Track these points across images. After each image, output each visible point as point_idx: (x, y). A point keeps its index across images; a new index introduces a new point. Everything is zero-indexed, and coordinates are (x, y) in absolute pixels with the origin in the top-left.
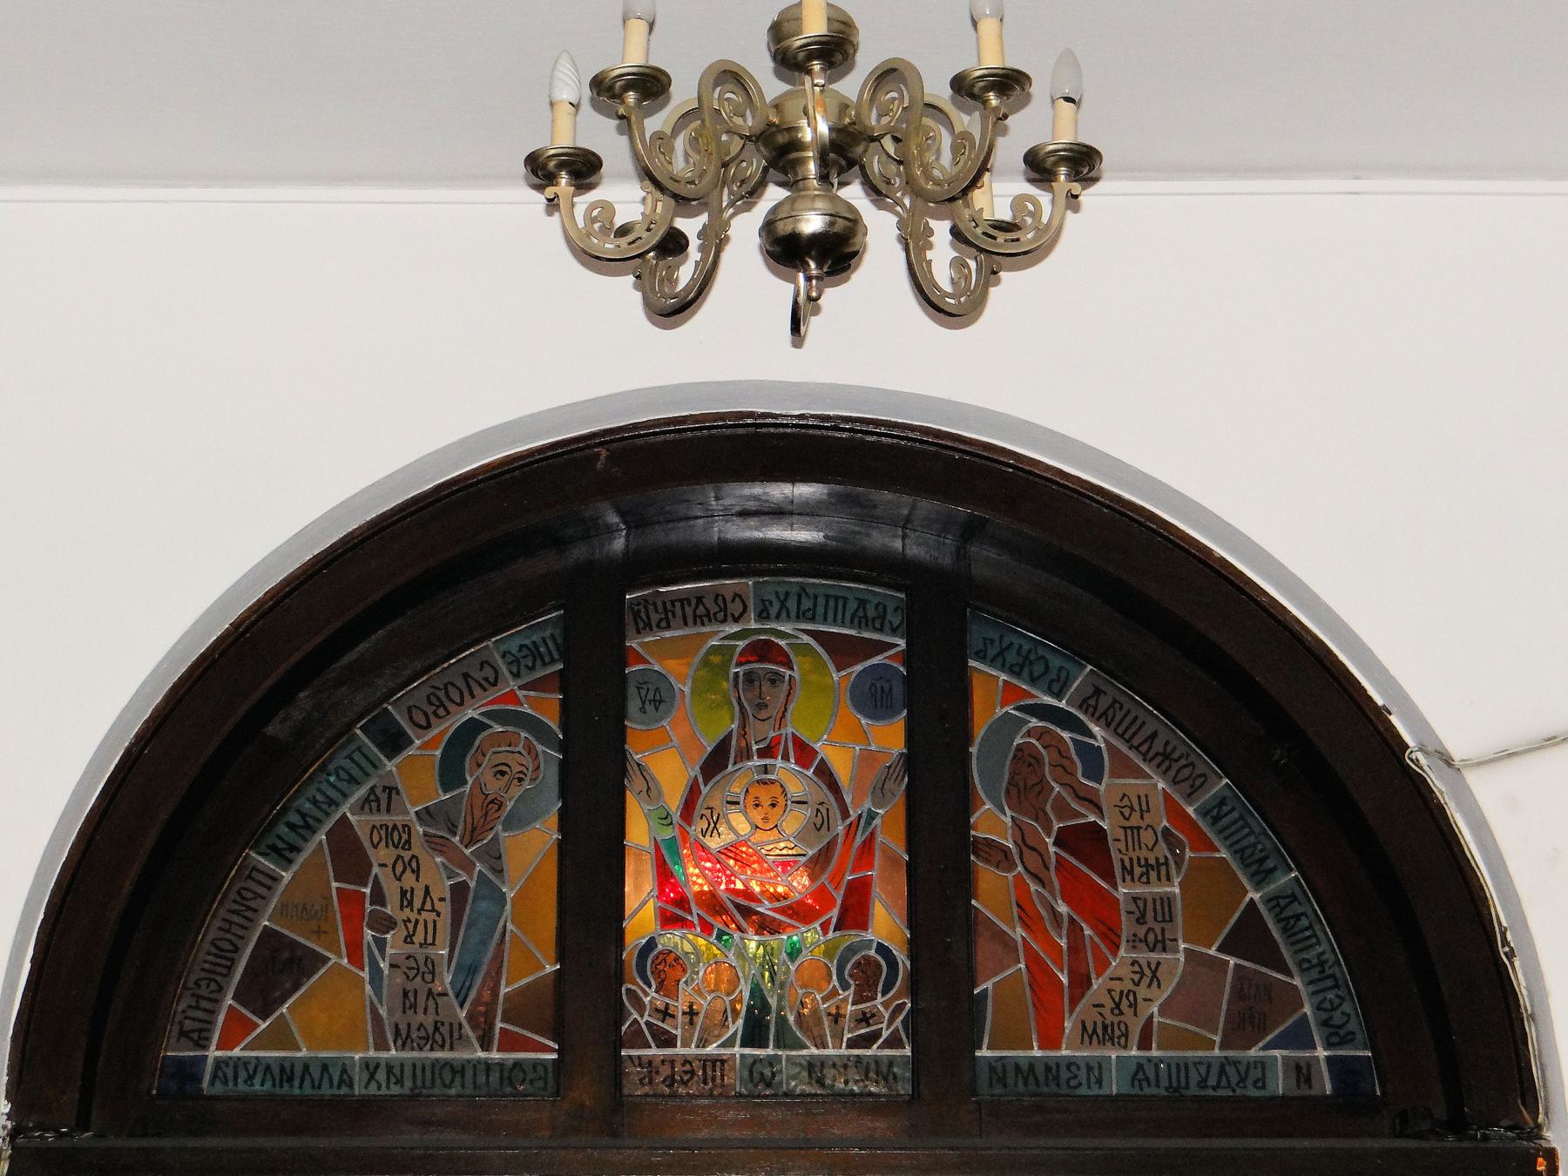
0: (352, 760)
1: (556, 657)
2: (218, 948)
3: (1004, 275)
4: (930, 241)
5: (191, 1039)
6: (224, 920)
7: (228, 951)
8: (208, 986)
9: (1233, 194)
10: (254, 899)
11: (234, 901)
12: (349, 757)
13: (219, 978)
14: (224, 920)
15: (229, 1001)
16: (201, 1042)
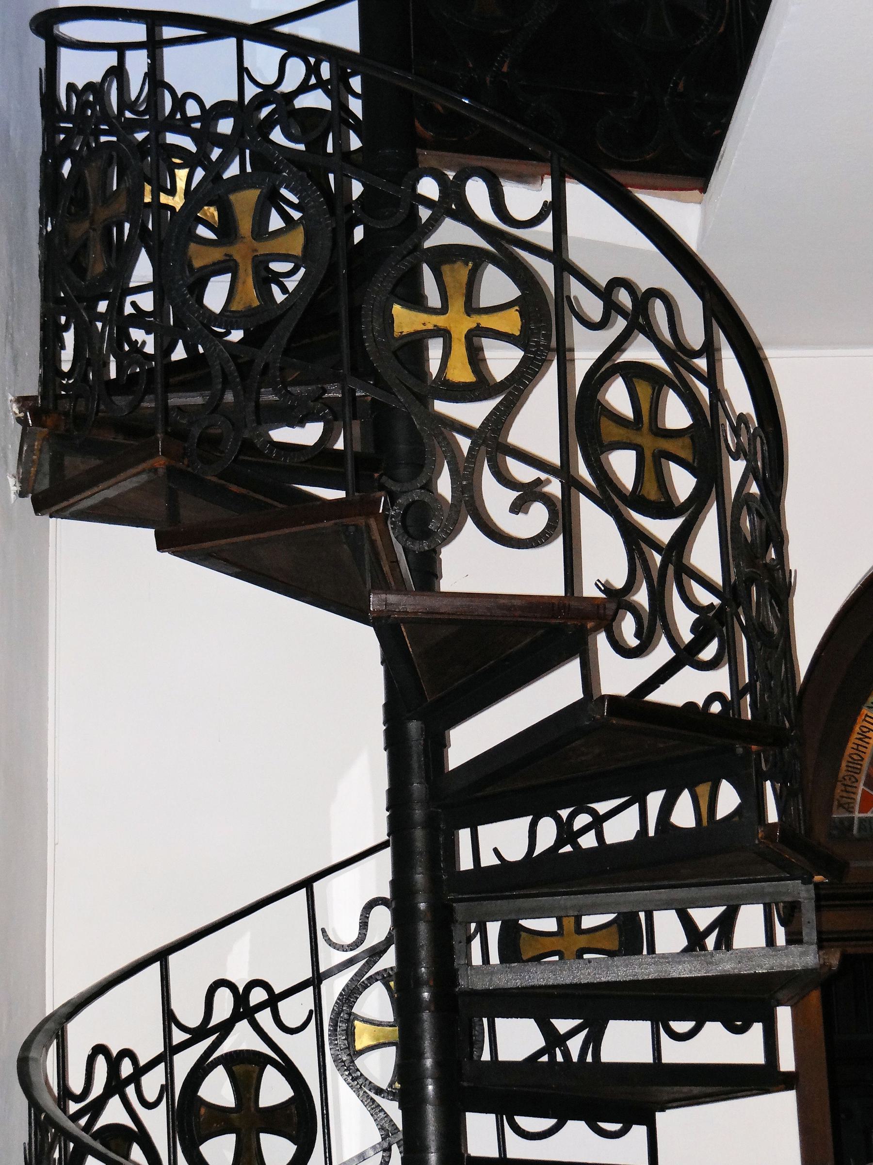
0: (867, 721)
1: (787, 1062)
2: (852, 758)
3: (245, 66)
4: (151, 334)
5: (844, 808)
6: (854, 743)
7: (859, 760)
8: (850, 779)
9: (506, 359)
10: (869, 732)
11: (858, 733)
12: (865, 720)
13: (856, 775)
14: (854, 743)
15: (861, 787)
16: (849, 809)
